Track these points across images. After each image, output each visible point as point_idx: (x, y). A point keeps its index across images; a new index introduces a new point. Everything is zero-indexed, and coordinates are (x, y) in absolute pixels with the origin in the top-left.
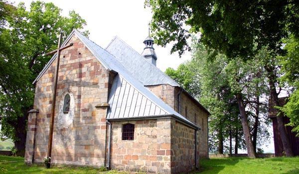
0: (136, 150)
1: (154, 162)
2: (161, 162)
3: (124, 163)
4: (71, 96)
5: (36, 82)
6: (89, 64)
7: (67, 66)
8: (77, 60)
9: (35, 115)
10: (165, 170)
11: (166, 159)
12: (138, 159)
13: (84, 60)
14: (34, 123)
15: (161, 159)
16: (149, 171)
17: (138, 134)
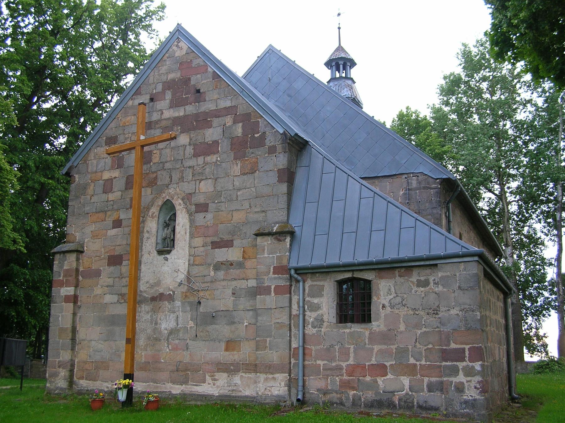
0: (380, 351)
1: (433, 379)
2: (455, 380)
3: (346, 385)
4: (177, 207)
5: (71, 168)
6: (229, 120)
7: (164, 124)
8: (190, 109)
9: (73, 257)
10: (466, 402)
11: (469, 372)
12: (386, 375)
13: (212, 106)
14: (72, 279)
15: (455, 371)
16: (420, 407)
17: (384, 306)
